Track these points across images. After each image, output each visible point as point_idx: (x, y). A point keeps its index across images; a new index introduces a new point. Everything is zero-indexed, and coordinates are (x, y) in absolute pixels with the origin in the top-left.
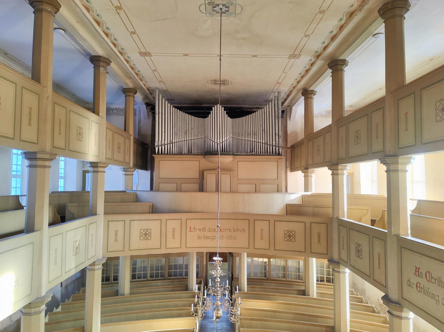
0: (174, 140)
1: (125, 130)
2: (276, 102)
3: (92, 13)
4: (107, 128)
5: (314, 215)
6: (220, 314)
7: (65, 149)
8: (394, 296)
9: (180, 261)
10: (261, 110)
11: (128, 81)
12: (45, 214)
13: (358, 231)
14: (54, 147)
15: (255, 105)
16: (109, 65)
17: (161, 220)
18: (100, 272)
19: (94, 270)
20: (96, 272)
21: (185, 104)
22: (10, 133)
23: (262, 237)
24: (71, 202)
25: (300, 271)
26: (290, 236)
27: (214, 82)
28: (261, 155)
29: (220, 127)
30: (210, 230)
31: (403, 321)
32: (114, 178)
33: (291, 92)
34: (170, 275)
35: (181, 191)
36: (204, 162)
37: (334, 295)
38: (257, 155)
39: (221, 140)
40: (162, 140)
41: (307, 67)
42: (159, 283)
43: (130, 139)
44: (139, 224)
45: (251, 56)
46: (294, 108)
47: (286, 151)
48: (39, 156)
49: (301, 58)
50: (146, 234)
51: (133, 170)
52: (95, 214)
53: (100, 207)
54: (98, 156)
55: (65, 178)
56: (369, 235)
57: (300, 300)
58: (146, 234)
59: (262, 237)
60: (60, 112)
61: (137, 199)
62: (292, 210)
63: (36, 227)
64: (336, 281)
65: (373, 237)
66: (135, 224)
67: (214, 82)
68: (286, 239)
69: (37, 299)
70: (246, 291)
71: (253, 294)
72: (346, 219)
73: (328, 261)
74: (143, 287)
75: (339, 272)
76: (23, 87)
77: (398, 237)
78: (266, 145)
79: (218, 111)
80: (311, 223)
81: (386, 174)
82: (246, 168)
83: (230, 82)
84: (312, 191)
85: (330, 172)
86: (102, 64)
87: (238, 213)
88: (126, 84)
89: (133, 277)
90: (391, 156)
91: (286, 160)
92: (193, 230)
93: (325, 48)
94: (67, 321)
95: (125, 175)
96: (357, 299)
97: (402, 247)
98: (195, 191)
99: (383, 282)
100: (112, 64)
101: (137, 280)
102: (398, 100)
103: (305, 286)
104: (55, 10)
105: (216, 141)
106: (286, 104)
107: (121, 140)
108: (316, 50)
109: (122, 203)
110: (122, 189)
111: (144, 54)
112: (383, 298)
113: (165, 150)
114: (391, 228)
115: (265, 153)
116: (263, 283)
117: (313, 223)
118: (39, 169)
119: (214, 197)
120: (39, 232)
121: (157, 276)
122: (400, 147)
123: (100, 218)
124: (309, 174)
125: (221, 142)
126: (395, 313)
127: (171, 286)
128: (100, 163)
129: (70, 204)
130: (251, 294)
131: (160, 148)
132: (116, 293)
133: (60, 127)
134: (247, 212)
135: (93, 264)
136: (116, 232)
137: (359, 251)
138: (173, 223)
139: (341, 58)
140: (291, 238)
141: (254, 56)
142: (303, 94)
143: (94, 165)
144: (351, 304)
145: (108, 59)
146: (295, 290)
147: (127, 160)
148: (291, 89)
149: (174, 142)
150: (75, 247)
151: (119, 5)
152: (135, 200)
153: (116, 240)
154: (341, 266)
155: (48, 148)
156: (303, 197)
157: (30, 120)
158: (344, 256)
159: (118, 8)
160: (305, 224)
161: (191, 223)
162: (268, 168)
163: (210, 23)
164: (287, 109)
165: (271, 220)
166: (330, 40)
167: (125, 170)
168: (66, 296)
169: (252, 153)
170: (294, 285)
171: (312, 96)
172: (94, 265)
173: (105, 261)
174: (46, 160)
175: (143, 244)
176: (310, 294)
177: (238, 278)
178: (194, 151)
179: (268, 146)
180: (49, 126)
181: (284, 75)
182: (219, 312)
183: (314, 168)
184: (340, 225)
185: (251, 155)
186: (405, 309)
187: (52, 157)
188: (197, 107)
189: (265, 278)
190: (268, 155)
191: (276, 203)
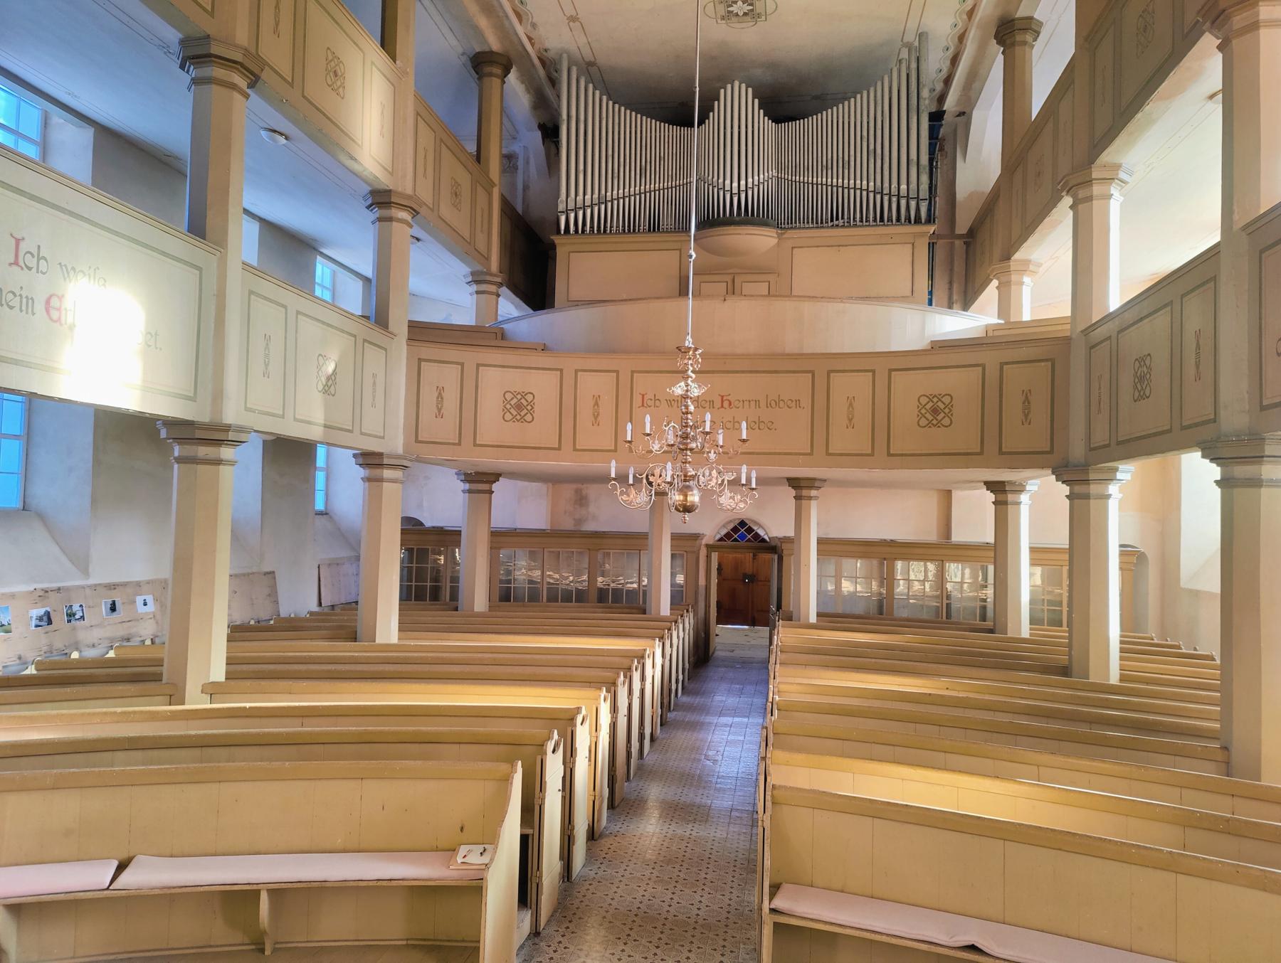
0: (609, 194)
2: (914, 65)
4: (418, 114)
17: (561, 370)
23: (850, 420)
26: (935, 411)
29: (742, 151)
33: (962, 38)
39: (743, 182)
40: (577, 192)
43: (490, 194)
46: (977, 115)
50: (520, 407)
58: (519, 407)
59: (850, 420)
78: (878, 197)
91: (951, 283)
92: (650, 403)
95: (477, 292)
105: (728, 188)
117: (1007, 363)
125: (743, 188)
133: (277, 15)
149: (609, 198)
153: (439, 413)
160: (984, 369)
171: (1029, 38)
175: (512, 433)
179: (886, 198)
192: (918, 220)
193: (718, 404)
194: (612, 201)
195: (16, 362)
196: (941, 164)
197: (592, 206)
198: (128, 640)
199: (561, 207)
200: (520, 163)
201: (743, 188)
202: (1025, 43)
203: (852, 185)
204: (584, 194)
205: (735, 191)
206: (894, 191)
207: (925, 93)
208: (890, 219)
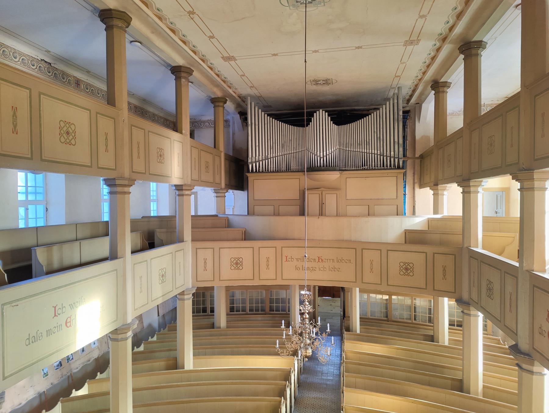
0: (269, 155)
1: (215, 147)
2: (396, 101)
3: (165, 22)
5: (441, 243)
6: (309, 353)
7: (145, 173)
8: (524, 345)
9: (283, 294)
10: (378, 111)
11: (215, 89)
12: (128, 241)
13: (489, 265)
14: (133, 172)
15: (372, 105)
16: (192, 75)
18: (190, 302)
19: (184, 300)
20: (186, 302)
21: (285, 110)
22: (88, 162)
23: (372, 270)
24: (160, 228)
25: (417, 310)
26: (407, 269)
27: (314, 83)
28: (375, 169)
29: (324, 138)
30: (309, 260)
31: (535, 377)
32: (205, 201)
33: (417, 86)
34: (271, 309)
35: (279, 215)
36: (306, 180)
37: (463, 341)
38: (370, 170)
39: (325, 153)
40: (256, 155)
41: (433, 54)
42: (259, 317)
43: (220, 157)
44: (229, 252)
45: (354, 48)
46: (424, 106)
47: (414, 162)
48: (118, 182)
49: (421, 43)
50: (237, 264)
51: (225, 191)
52: (182, 241)
53: (188, 234)
54: (182, 178)
55: (157, 201)
56: (501, 270)
57: (426, 346)
58: (237, 264)
59: (372, 270)
60: (138, 135)
61: (228, 224)
62: (413, 238)
63: (119, 254)
64: (464, 325)
65: (505, 272)
66: (224, 252)
67: (314, 83)
68: (402, 273)
69: (123, 325)
70: (358, 332)
71: (367, 336)
72: (480, 250)
73: (456, 301)
74: (242, 320)
75: (469, 315)
76: (97, 113)
77: (530, 272)
78: (382, 157)
79: (321, 118)
80: (434, 254)
81: (519, 192)
82: (356, 186)
83: (334, 81)
84: (443, 214)
85: (461, 190)
86: (183, 74)
87: (343, 240)
88: (214, 93)
89: (232, 309)
90: (525, 170)
91: (414, 173)
93: (451, 29)
94: (161, 351)
95: (217, 197)
96: (503, 350)
97: (534, 286)
98: (295, 215)
99: (514, 328)
100: (195, 73)
101: (235, 313)
102: (535, 96)
103: (433, 330)
104: (126, 24)
105: (318, 155)
106: (413, 100)
107: (208, 158)
108: (440, 32)
109: (213, 229)
110: (214, 213)
111: (228, 59)
112: (511, 347)
113: (259, 167)
114: (523, 262)
115: (380, 166)
116: (380, 324)
118: (119, 196)
119: (324, 221)
120: (122, 259)
121: (257, 310)
122: (536, 158)
123: (188, 245)
124: (440, 192)
125: (325, 155)
126: (524, 366)
127: (271, 322)
128: (185, 185)
129: (158, 230)
130: (363, 336)
131: (254, 165)
132: (212, 326)
133: (138, 150)
134: (353, 239)
135: (182, 293)
136: (205, 260)
137: (490, 289)
138: (267, 251)
139: (476, 39)
140: (408, 272)
141: (358, 48)
142: (433, 88)
143: (179, 188)
144: (484, 354)
145: (189, 68)
146: (421, 335)
147: (217, 180)
148: (416, 83)
149: (269, 157)
150: (163, 277)
151: (192, 10)
152: (227, 226)
153: (205, 269)
154: (472, 308)
155: (127, 174)
156: (429, 221)
157: (107, 146)
158: (475, 296)
159: (191, 13)
161: (286, 252)
162: (385, 185)
163: (294, 18)
164: (415, 108)
165: (384, 249)
166: (455, 18)
167: (216, 192)
168: (162, 326)
169: (364, 166)
170: (420, 328)
171: (445, 89)
172: (184, 295)
173: (194, 291)
174: (125, 186)
176: (440, 341)
177: (349, 317)
178: (293, 166)
179: (385, 158)
180: (126, 151)
181: (402, 66)
182: (308, 351)
183: (447, 183)
184: (471, 257)
185: (363, 170)
186: (536, 363)
187: (131, 182)
188: (295, 114)
189: (386, 319)
190: (384, 169)
191: (392, 228)
192: (399, 168)
193: (317, 260)
194: (270, 158)
195: (57, 351)
196: (408, 122)
197: (262, 160)
198: (89, 361)
199: (250, 161)
200: (231, 124)
201: (325, 155)
202: (443, 92)
203: (370, 152)
204: (259, 156)
205: (322, 156)
206: (388, 154)
207: (401, 102)
208: (387, 166)
